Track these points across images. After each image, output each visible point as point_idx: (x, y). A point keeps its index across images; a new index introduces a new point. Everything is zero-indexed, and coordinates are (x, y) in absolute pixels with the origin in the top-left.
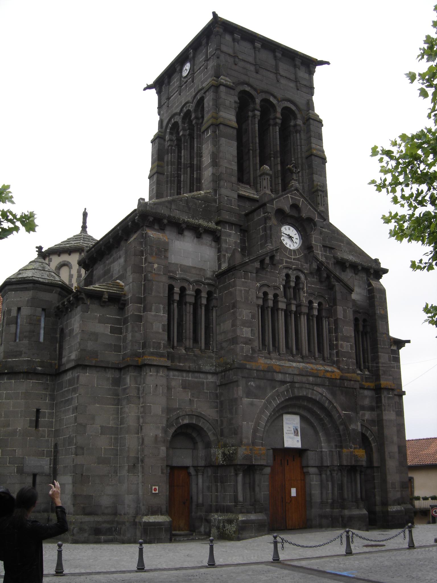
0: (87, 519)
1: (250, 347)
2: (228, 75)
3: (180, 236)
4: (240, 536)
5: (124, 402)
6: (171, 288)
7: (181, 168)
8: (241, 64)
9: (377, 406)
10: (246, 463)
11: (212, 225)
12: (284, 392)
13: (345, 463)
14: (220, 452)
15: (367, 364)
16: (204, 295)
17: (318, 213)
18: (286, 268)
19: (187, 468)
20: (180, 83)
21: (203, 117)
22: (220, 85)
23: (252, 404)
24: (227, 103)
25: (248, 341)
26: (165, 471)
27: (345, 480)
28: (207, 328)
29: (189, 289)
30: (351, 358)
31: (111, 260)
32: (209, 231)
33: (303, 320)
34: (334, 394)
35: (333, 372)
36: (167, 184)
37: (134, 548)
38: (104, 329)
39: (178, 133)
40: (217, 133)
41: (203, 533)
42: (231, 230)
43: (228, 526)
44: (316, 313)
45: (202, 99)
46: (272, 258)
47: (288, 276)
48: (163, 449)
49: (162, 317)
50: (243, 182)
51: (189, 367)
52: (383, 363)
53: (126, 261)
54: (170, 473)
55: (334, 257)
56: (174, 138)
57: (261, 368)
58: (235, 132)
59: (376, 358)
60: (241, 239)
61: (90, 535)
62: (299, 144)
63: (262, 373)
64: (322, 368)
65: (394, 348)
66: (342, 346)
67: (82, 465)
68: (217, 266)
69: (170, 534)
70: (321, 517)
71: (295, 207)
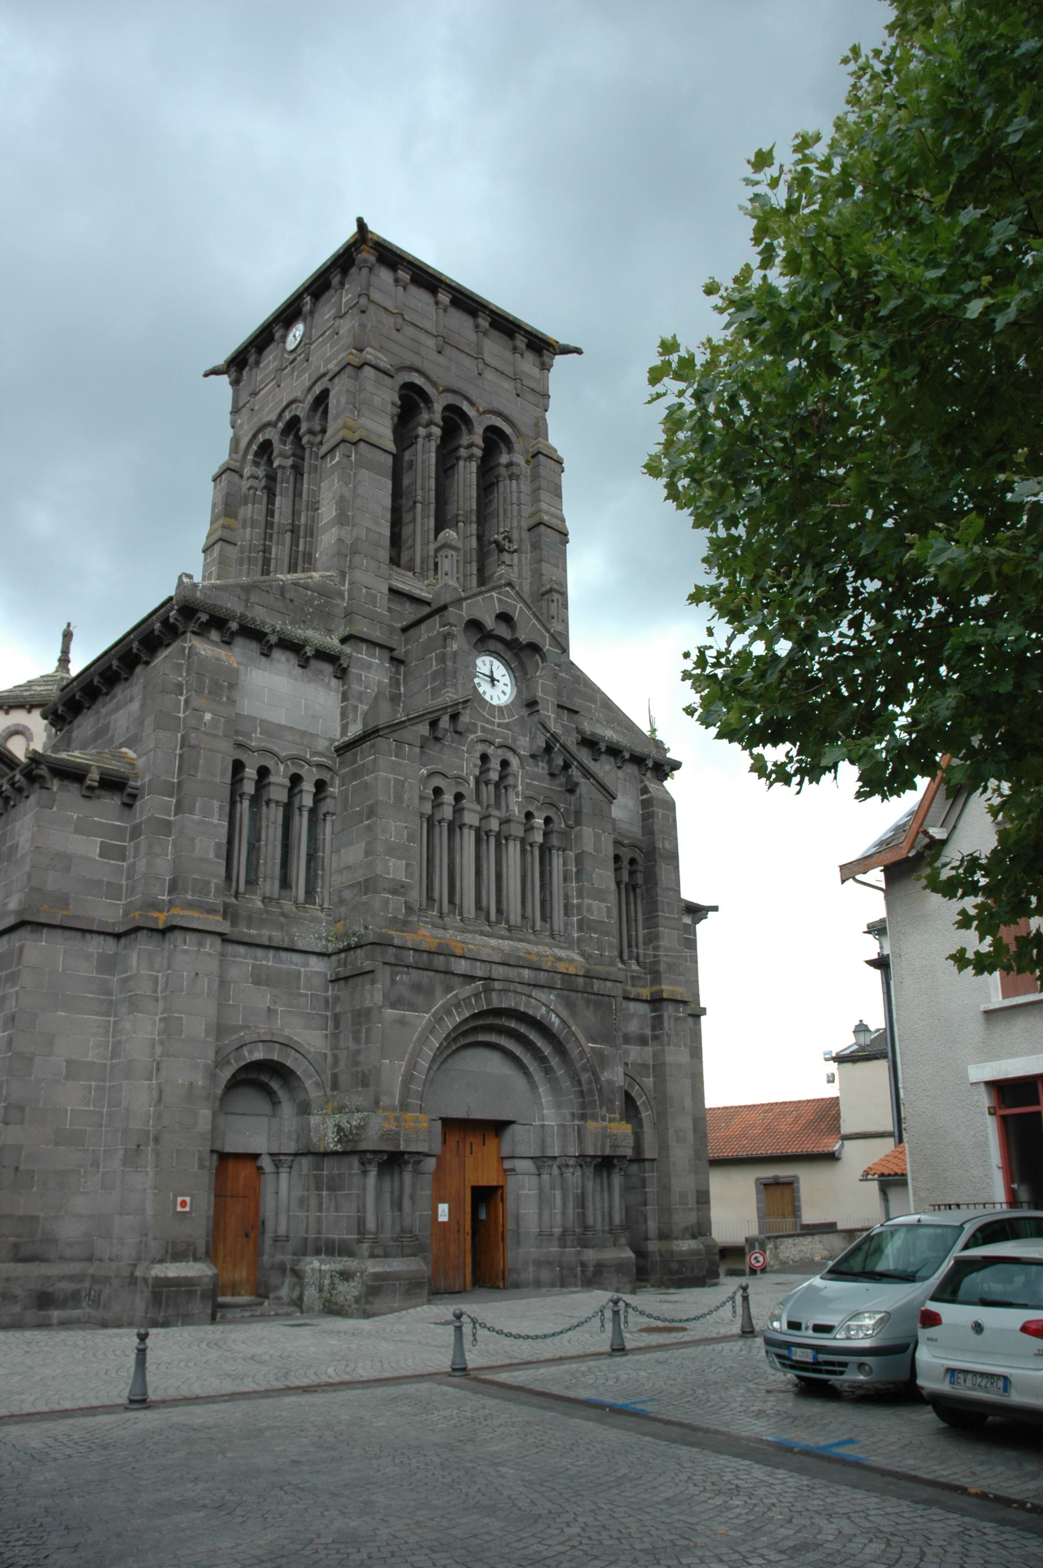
0: (21, 1268)
1: (402, 899)
2: (381, 349)
3: (263, 659)
4: (368, 1307)
5: (123, 1009)
6: (238, 767)
7: (271, 535)
8: (409, 331)
9: (655, 1033)
10: (386, 1148)
11: (333, 642)
12: (469, 998)
13: (590, 1152)
14: (330, 1123)
15: (635, 950)
16: (308, 786)
17: (552, 635)
18: (483, 741)
19: (256, 1156)
20: (281, 363)
21: (324, 431)
22: (365, 364)
23: (402, 1022)
24: (377, 401)
25: (399, 889)
26: (207, 1163)
27: (590, 1185)
28: (311, 857)
29: (278, 772)
30: (608, 934)
31: (111, 706)
32: (325, 656)
33: (513, 850)
34: (570, 1006)
35: (571, 961)
36: (241, 565)
37: (127, 1339)
38: (90, 847)
39: (270, 462)
40: (353, 458)
41: (286, 1299)
42: (373, 656)
43: (342, 1287)
44: (539, 838)
45: (325, 394)
46: (454, 717)
47: (484, 758)
48: (205, 1114)
49: (215, 826)
50: (398, 566)
51: (270, 938)
52: (667, 950)
53: (143, 706)
54: (217, 1168)
55: (579, 731)
56: (261, 472)
57: (424, 946)
58: (390, 460)
59: (652, 939)
60: (391, 678)
61: (25, 1308)
62: (515, 500)
63: (425, 956)
64: (548, 951)
65: (687, 920)
66: (589, 910)
67: (19, 1148)
68: (339, 729)
69: (214, 1304)
70: (539, 1263)
71: (504, 617)
